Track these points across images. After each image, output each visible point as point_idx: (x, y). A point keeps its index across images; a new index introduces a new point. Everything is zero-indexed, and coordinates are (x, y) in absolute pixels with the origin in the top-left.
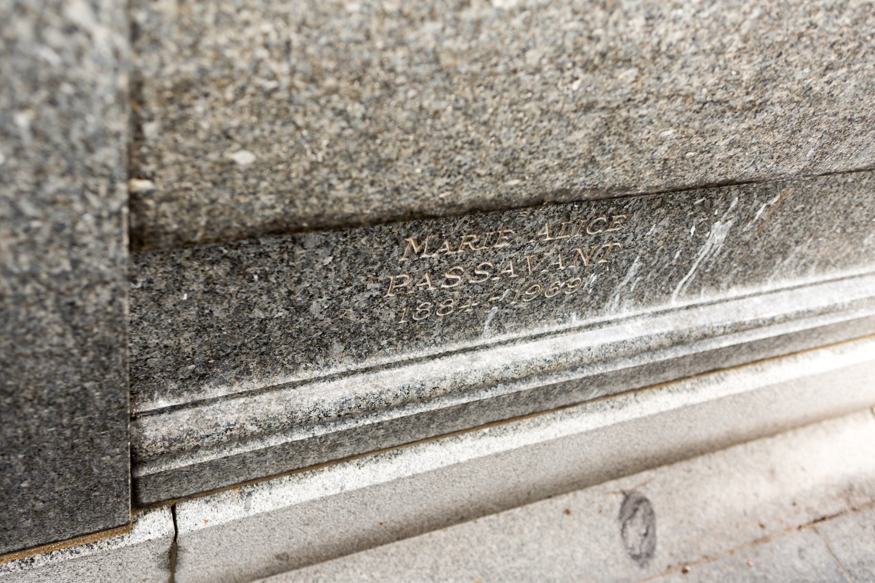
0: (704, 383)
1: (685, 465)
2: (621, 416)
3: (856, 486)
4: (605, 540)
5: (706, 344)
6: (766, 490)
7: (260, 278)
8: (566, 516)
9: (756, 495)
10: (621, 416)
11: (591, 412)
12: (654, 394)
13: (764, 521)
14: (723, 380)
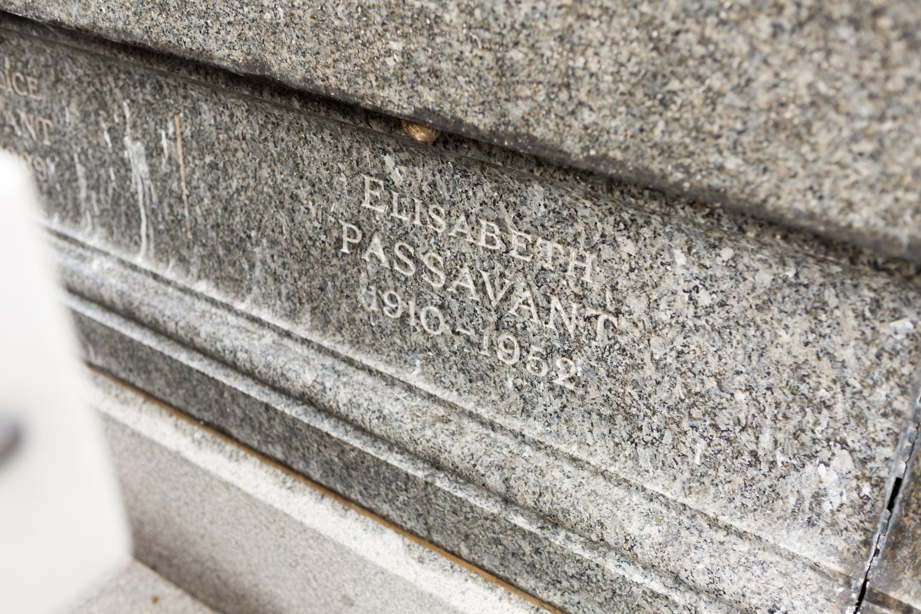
0: (216, 446)
5: (176, 351)
7: (279, 256)
8: (149, 601)
11: (98, 385)
12: (161, 414)
14: (237, 460)
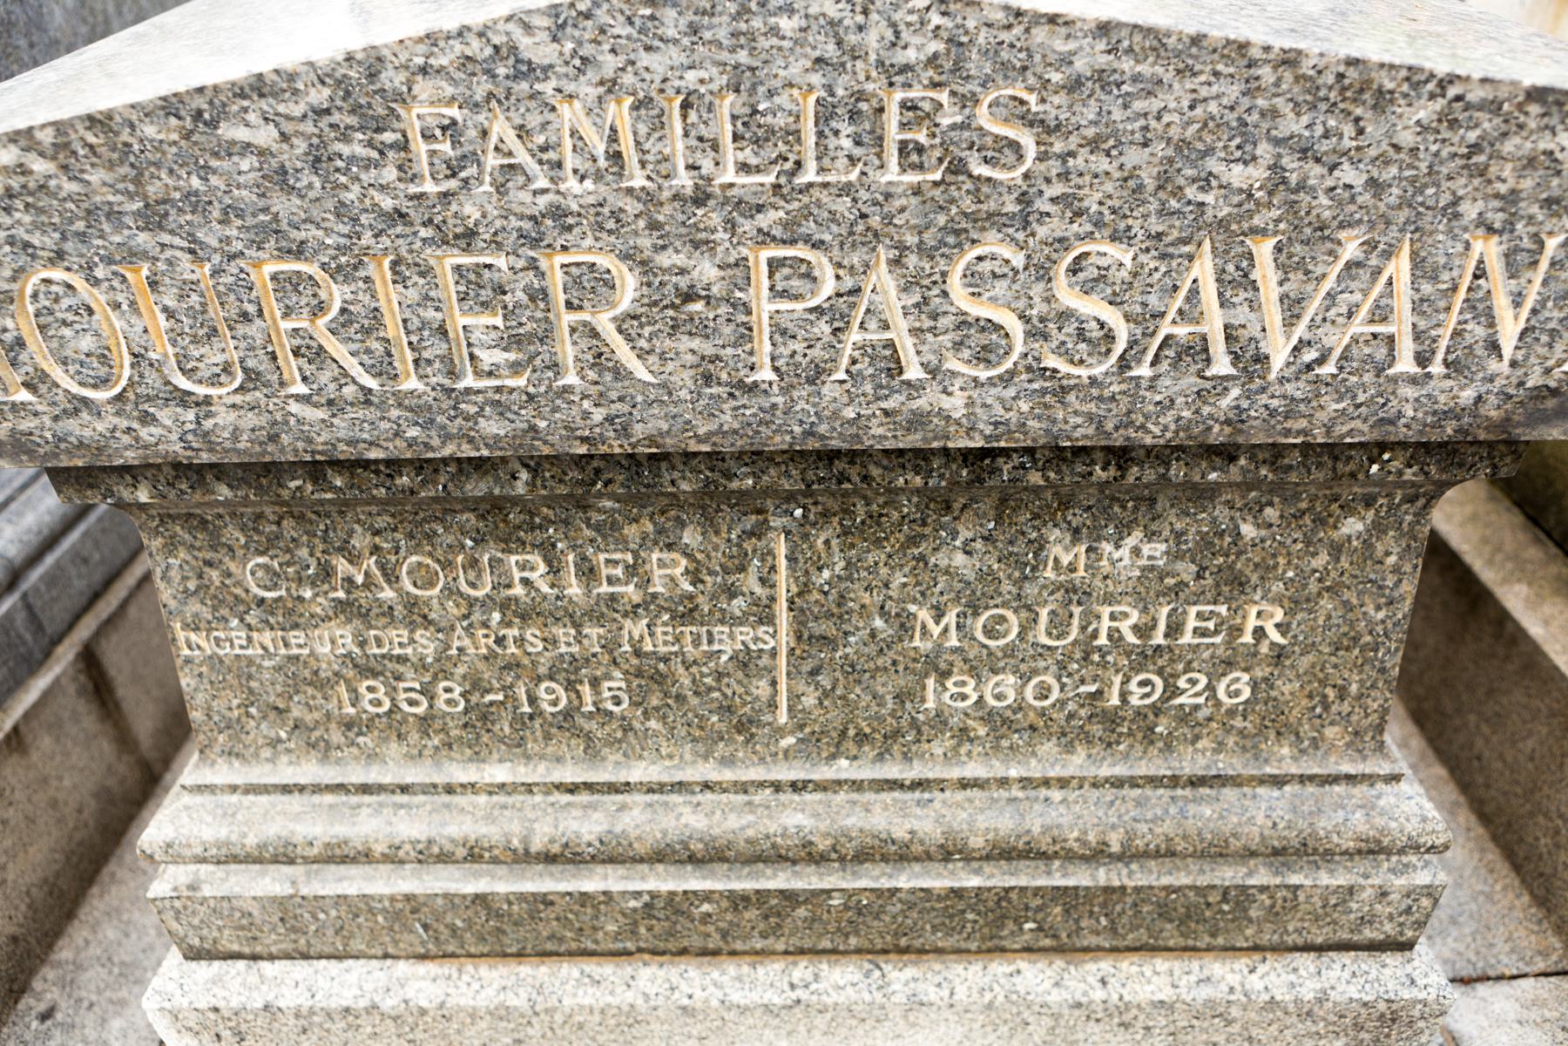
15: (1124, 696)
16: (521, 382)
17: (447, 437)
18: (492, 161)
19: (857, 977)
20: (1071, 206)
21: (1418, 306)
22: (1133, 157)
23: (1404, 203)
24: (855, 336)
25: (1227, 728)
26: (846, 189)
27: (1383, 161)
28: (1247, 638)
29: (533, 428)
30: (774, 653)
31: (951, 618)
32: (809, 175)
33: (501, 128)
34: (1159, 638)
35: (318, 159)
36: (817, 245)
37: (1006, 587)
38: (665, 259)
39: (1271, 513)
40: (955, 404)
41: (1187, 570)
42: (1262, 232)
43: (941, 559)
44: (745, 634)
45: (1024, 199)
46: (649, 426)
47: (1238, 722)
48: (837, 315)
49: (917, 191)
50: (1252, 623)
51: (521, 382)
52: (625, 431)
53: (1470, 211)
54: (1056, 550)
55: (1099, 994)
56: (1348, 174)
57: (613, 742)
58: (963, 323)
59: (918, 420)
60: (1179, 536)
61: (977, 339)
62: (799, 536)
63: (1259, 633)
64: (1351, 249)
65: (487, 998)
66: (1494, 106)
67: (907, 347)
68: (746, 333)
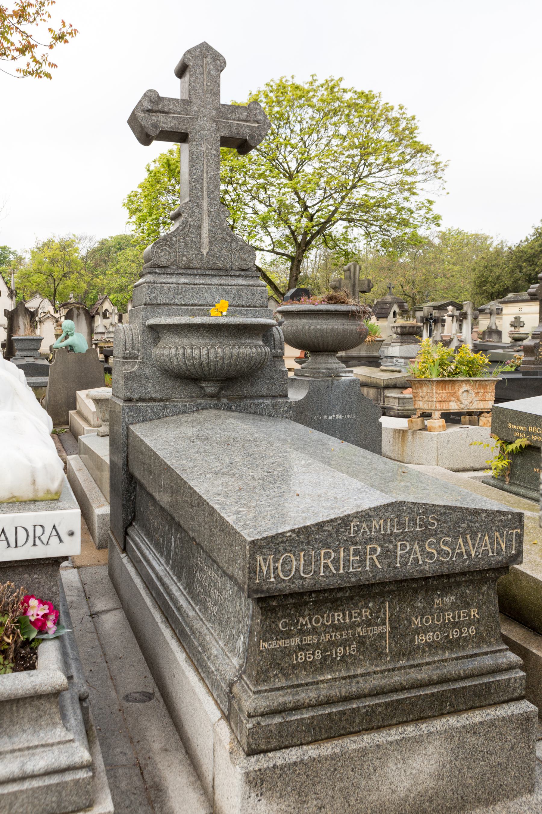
1: (167, 714)
2: (153, 610)
3: (160, 794)
4: (135, 687)
6: (156, 746)
9: (154, 741)
10: (153, 610)
13: (141, 743)
15: (453, 635)
16: (360, 570)
17: (345, 582)
18: (362, 531)
19: (414, 728)
20: (442, 532)
21: (491, 544)
22: (450, 524)
23: (485, 528)
24: (412, 557)
25: (473, 642)
26: (412, 532)
27: (481, 522)
28: (472, 617)
29: (360, 579)
30: (386, 633)
31: (419, 619)
32: (406, 530)
33: (364, 525)
34: (457, 620)
35: (337, 532)
36: (407, 541)
37: (428, 610)
38: (385, 545)
39: (471, 587)
40: (427, 568)
41: (459, 601)
42: (467, 534)
43: (416, 605)
44: (380, 628)
45: (436, 531)
46: (379, 576)
47: (475, 640)
48: (409, 553)
49: (421, 531)
50: (472, 613)
51: (360, 570)
52: (375, 578)
53: (494, 528)
54: (436, 600)
55: (468, 722)
56: (477, 524)
57: (353, 664)
58: (428, 552)
59: (421, 571)
60: (456, 594)
61: (430, 555)
62: (391, 602)
63: (474, 616)
64: (480, 536)
65: (330, 752)
66: (493, 513)
67: (420, 557)
68: (396, 557)
